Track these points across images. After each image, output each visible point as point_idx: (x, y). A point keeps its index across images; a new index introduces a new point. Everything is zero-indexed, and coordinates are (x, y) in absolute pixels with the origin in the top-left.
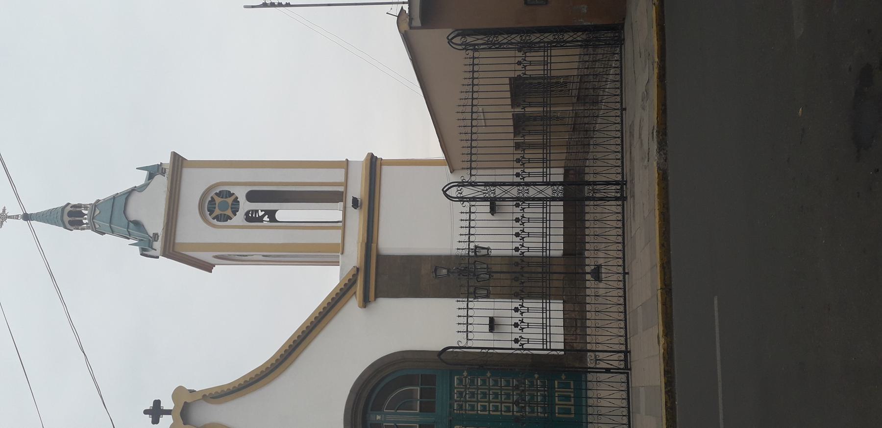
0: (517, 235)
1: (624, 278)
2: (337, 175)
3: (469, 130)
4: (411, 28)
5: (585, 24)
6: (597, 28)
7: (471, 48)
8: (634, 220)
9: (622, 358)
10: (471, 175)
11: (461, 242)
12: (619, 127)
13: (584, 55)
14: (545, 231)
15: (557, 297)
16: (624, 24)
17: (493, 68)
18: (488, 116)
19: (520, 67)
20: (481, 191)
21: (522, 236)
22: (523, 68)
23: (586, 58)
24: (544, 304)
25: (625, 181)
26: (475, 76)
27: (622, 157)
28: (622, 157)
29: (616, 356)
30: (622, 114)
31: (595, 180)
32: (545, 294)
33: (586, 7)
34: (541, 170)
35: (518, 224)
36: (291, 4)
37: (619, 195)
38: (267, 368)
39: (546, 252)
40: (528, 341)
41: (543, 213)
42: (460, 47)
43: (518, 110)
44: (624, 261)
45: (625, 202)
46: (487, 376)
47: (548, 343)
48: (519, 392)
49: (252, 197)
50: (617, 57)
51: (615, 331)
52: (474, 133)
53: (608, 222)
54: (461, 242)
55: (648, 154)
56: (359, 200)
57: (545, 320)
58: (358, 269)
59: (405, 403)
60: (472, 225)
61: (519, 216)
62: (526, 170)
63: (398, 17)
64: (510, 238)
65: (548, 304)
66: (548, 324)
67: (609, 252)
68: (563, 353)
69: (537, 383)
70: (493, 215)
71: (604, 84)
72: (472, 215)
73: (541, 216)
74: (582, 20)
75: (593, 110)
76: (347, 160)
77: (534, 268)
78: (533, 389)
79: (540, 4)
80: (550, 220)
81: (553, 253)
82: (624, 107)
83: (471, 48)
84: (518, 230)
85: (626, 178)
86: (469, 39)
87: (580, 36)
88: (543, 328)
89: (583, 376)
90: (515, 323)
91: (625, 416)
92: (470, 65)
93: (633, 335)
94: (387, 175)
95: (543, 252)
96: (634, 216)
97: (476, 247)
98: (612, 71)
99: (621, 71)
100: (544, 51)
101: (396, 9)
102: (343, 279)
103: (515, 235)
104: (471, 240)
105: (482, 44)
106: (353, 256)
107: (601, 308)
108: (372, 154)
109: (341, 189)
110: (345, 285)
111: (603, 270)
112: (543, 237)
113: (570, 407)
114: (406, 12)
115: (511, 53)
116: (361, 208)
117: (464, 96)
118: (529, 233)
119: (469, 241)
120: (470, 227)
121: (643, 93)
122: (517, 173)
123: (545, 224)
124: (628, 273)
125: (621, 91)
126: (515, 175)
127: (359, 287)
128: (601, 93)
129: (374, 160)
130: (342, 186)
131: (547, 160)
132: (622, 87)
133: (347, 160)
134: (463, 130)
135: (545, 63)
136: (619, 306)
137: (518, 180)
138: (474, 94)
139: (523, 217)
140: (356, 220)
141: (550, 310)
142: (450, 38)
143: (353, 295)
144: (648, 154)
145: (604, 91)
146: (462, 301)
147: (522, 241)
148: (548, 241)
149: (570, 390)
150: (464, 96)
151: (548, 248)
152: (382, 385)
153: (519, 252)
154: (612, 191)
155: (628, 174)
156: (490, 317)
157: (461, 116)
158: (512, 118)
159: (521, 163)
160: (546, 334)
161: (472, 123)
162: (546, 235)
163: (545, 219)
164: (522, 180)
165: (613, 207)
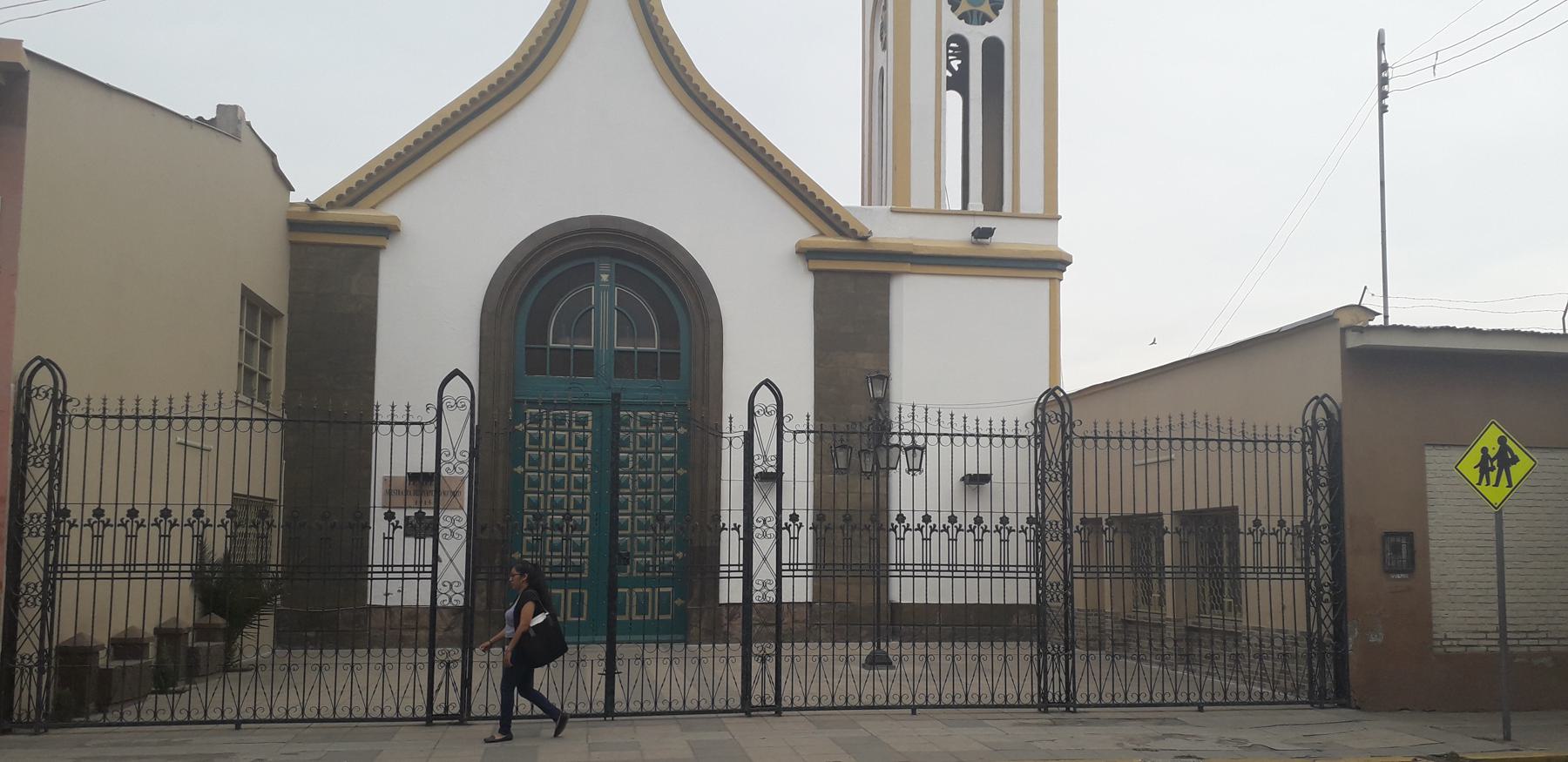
0: (927, 519)
1: (1193, 704)
2: (1031, 201)
3: (1164, 434)
4: (1343, 330)
5: (1350, 639)
6: (1341, 661)
7: (1038, 430)
8: (1015, 725)
9: (768, 702)
10: (1083, 438)
11: (965, 421)
12: (1170, 699)
13: (1284, 639)
14: (800, 567)
15: (818, 591)
16: (1351, 708)
17: (1102, 478)
18: (1165, 468)
19: (1274, 524)
20: (1054, 453)
21: (976, 529)
22: (1022, 527)
23: (1278, 643)
24: (804, 567)
25: (1075, 709)
26: (1137, 442)
27: (1118, 705)
28: (1118, 705)
29: (770, 691)
30: (1193, 704)
31: (1077, 658)
32: (1006, 568)
33: (1380, 640)
34: (1289, 563)
35: (997, 521)
36: (1385, 114)
37: (1050, 697)
38: (690, 78)
39: (896, 570)
40: (794, 538)
41: (913, 565)
42: (1308, 417)
43: (1167, 523)
44: (814, 709)
45: (1036, 710)
46: (679, 469)
47: (791, 573)
48: (651, 522)
49: (993, 49)
50: (1280, 696)
51: (814, 690)
52: (1158, 443)
53: (976, 680)
54: (965, 421)
55: (1147, 750)
56: (988, 240)
57: (400, 569)
58: (865, 239)
59: (628, 324)
60: (994, 439)
61: (1012, 524)
62: (1289, 537)
63: (1359, 306)
64: (919, 506)
65: (804, 573)
66: (796, 573)
67: (923, 682)
68: (369, 603)
69: (667, 556)
70: (963, 479)
71: (1222, 673)
72: (1012, 440)
73: (174, 559)
74: (1356, 633)
75: (964, 656)
76: (1059, 218)
77: (868, 550)
78: (658, 549)
79: (1384, 560)
80: (1004, 578)
81: (894, 582)
82: (1205, 708)
83: (1038, 430)
84: (986, 522)
85: (1080, 712)
86: (1322, 433)
87: (1328, 627)
88: (383, 566)
89: (680, 637)
90: (170, 511)
91: (577, 707)
92: (1108, 431)
93: (811, 721)
94: (1031, 290)
95: (896, 564)
96: (1020, 724)
97: (923, 449)
98: (1243, 687)
99: (1243, 703)
100: (1082, 566)
101: (1373, 303)
102: (847, 212)
103: (978, 516)
104: (929, 437)
105: (1314, 458)
106: (887, 229)
107: (827, 666)
108: (1071, 263)
109: (1007, 207)
110: (838, 217)
111: (883, 672)
112: (923, 565)
113: (627, 611)
114: (1370, 320)
115: (1299, 510)
116: (973, 243)
117: (1225, 425)
118: (982, 540)
119: (939, 434)
120: (978, 436)
121: (1247, 741)
122: (1008, 519)
123: (972, 569)
124: (914, 713)
125: (1233, 704)
126: (1004, 516)
127: (834, 242)
128: (1205, 670)
129: (1060, 266)
130: (1013, 211)
131: (130, 572)
132: (835, 708)
133: (1059, 218)
134: (1164, 423)
135: (1281, 569)
136: (830, 698)
137: (785, 519)
138: (1000, 439)
139: (1010, 531)
140: (954, 235)
141: (387, 579)
142: (1326, 400)
143: (819, 230)
144: (1147, 750)
145: (1208, 673)
146: (808, 423)
147: (968, 528)
148: (968, 574)
149: (656, 614)
150: (1225, 425)
151: (955, 574)
152: (665, 288)
153: (896, 523)
154: (1056, 689)
155: (1087, 715)
156: (991, 474)
157: (1188, 419)
158: (1210, 506)
159: (1253, 528)
160: (729, 571)
161: (1200, 439)
162: (926, 571)
163: (132, 569)
164: (1074, 529)
165: (1029, 690)
